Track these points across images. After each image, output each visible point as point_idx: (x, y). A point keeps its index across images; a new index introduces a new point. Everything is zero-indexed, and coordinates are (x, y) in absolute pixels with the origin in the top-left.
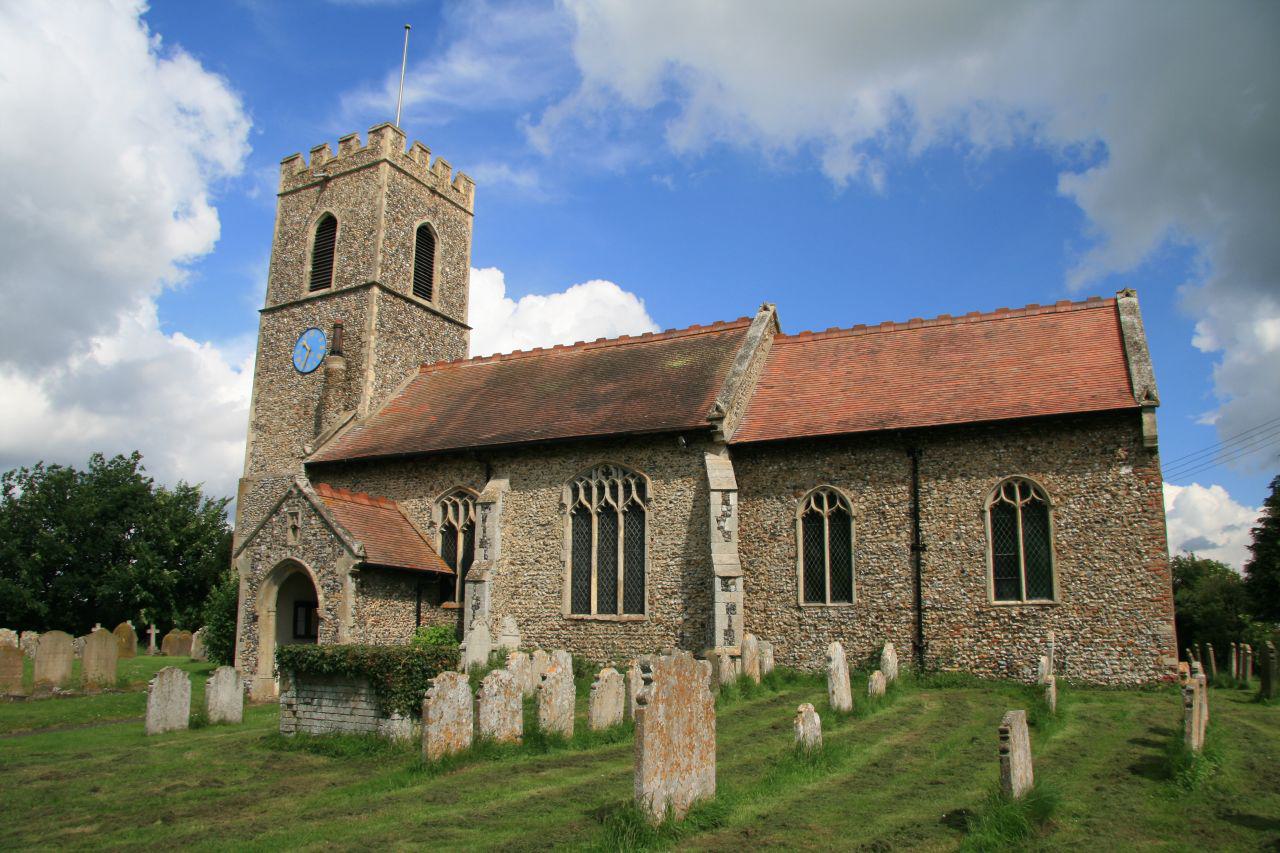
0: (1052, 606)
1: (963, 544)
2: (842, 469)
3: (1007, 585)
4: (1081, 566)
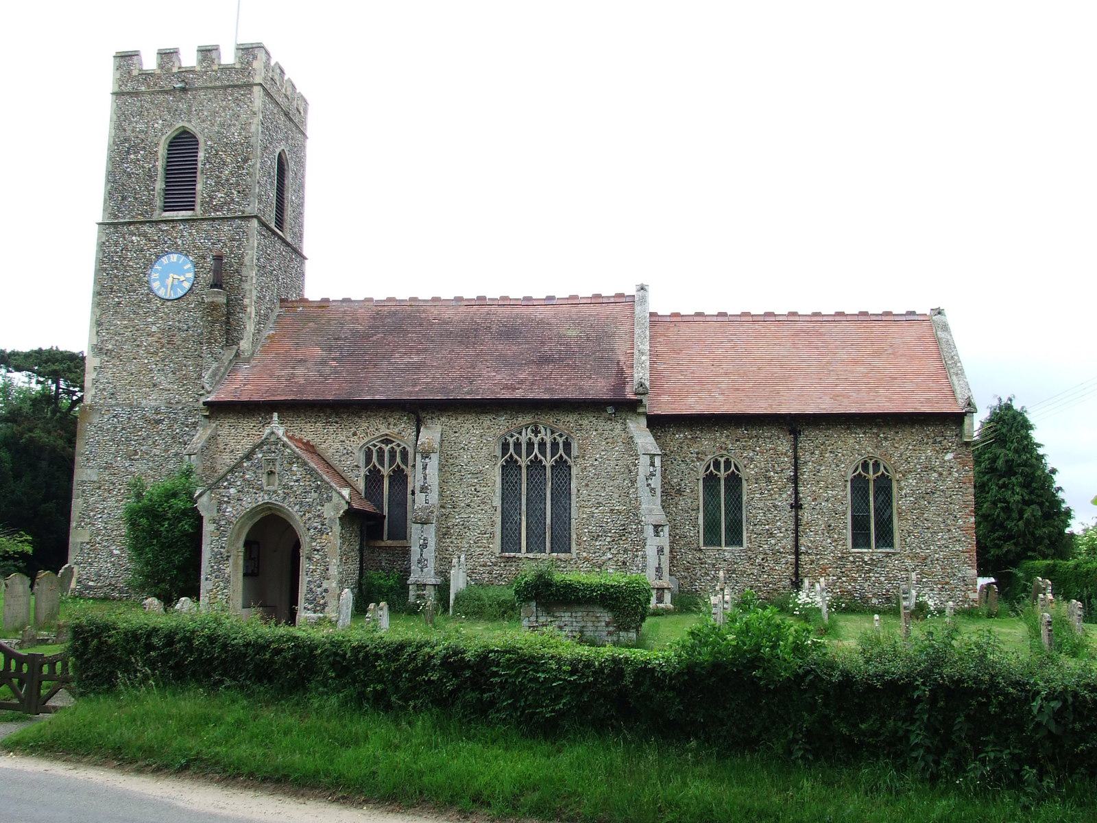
0: (894, 554)
1: (830, 505)
2: (737, 441)
3: (861, 537)
4: (915, 525)
